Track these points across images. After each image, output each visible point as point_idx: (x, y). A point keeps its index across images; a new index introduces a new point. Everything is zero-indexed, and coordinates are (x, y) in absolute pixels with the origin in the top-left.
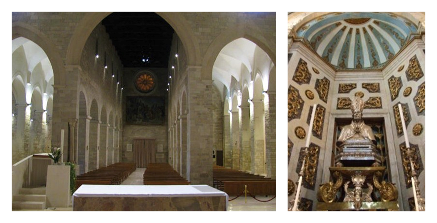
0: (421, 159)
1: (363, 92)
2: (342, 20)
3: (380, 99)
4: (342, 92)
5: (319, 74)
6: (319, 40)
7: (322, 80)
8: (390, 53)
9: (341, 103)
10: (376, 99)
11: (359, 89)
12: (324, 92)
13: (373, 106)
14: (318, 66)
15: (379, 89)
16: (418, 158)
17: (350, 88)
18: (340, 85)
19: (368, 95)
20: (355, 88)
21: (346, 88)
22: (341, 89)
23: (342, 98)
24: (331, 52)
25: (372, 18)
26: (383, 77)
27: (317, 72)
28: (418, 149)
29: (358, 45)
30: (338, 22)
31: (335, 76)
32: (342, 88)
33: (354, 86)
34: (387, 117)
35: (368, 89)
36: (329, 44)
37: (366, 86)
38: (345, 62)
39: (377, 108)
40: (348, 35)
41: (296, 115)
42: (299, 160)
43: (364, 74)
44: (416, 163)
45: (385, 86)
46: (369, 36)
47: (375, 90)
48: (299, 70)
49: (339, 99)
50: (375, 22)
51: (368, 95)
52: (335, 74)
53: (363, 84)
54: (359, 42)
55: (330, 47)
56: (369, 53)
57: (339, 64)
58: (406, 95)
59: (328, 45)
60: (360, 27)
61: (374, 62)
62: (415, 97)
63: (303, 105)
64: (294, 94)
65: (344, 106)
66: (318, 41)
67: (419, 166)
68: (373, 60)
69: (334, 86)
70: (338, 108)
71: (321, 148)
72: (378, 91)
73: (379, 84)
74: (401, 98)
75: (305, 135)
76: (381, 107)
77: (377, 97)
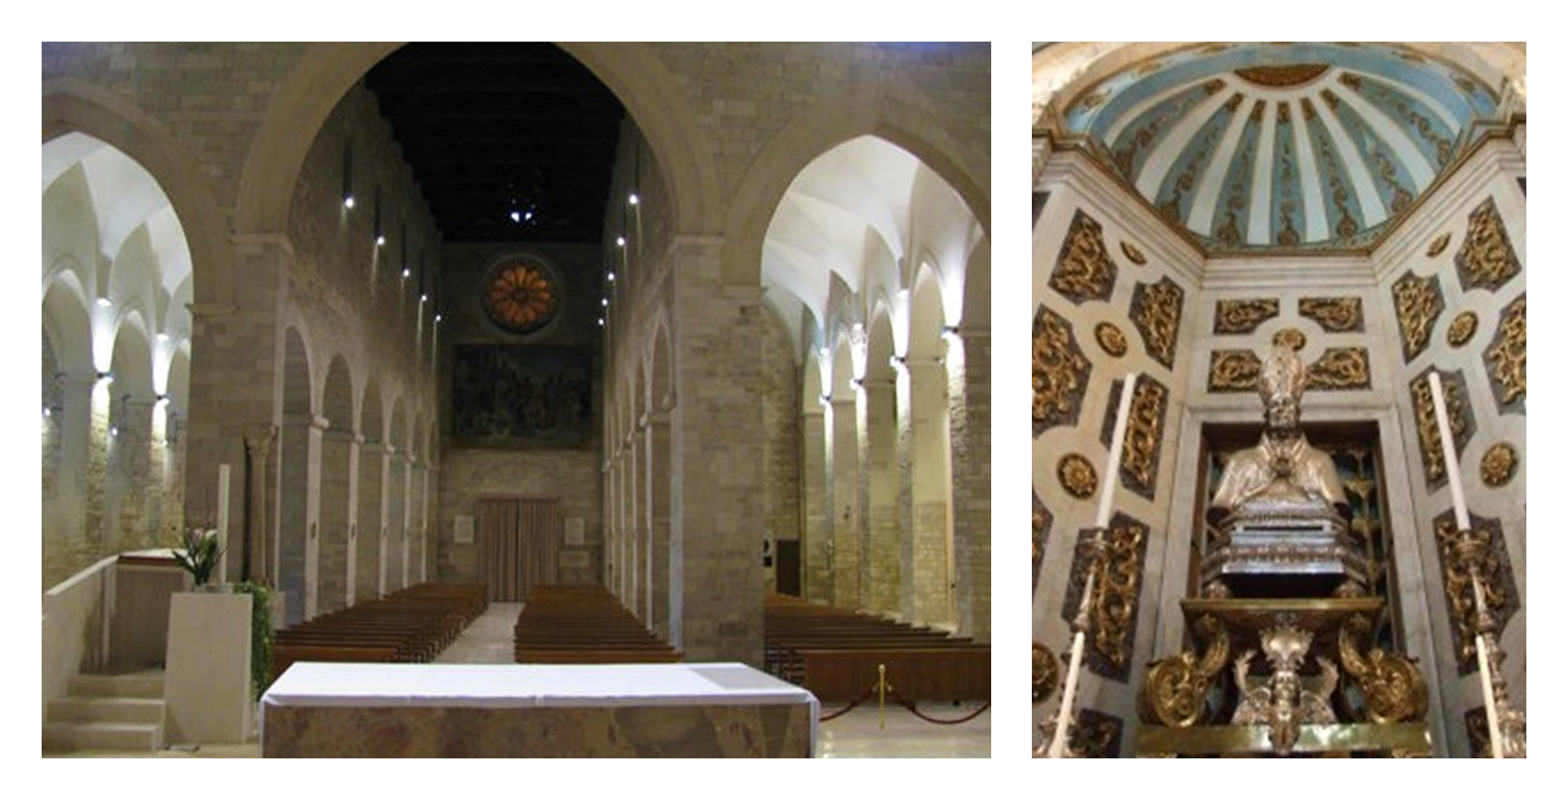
0: (1509, 570)
1: (1302, 329)
2: (1227, 70)
3: (1364, 353)
4: (1226, 332)
5: (1146, 267)
6: (1144, 144)
7: (1156, 287)
8: (1400, 191)
9: (1223, 368)
10: (1349, 357)
11: (1289, 318)
12: (1163, 330)
13: (1338, 382)
14: (1142, 237)
15: (1360, 319)
16: (1499, 567)
17: (1254, 315)
18: (1219, 305)
19: (1319, 342)
20: (1274, 314)
21: (1243, 317)
22: (1224, 319)
23: (1225, 352)
24: (1187, 188)
25: (1336, 64)
26: (1374, 276)
27: (1138, 260)
28: (1501, 535)
29: (1285, 161)
30: (1212, 78)
31: (1204, 271)
32: (1228, 314)
33: (1271, 309)
34: (1390, 418)
35: (1320, 320)
36: (1182, 157)
37: (1311, 309)
38: (1238, 223)
39: (1351, 386)
40: (1247, 124)
41: (1061, 412)
42: (1072, 576)
43: (1305, 265)
44: (1491, 586)
45: (1380, 310)
46: (1325, 129)
47: (1345, 322)
48: (1075, 250)
49: (1215, 355)
50: (1347, 80)
51: (1319, 342)
52: (1201, 265)
53: (1302, 302)
54: (1287, 151)
55: (1184, 170)
56: (1324, 189)
57: (1216, 228)
58: (1459, 339)
59: (1177, 163)
60: (1293, 96)
61: (1343, 222)
62: (1491, 347)
63: (1087, 377)
64: (1054, 336)
65: (1234, 380)
66: (1139, 147)
67: (1505, 596)
68: (1340, 217)
69: (1199, 309)
70: (1213, 389)
71: (1151, 531)
72: (1357, 326)
73: (1359, 301)
74: (1438, 352)
75: (1094, 486)
76: (1366, 385)
77: (1354, 349)
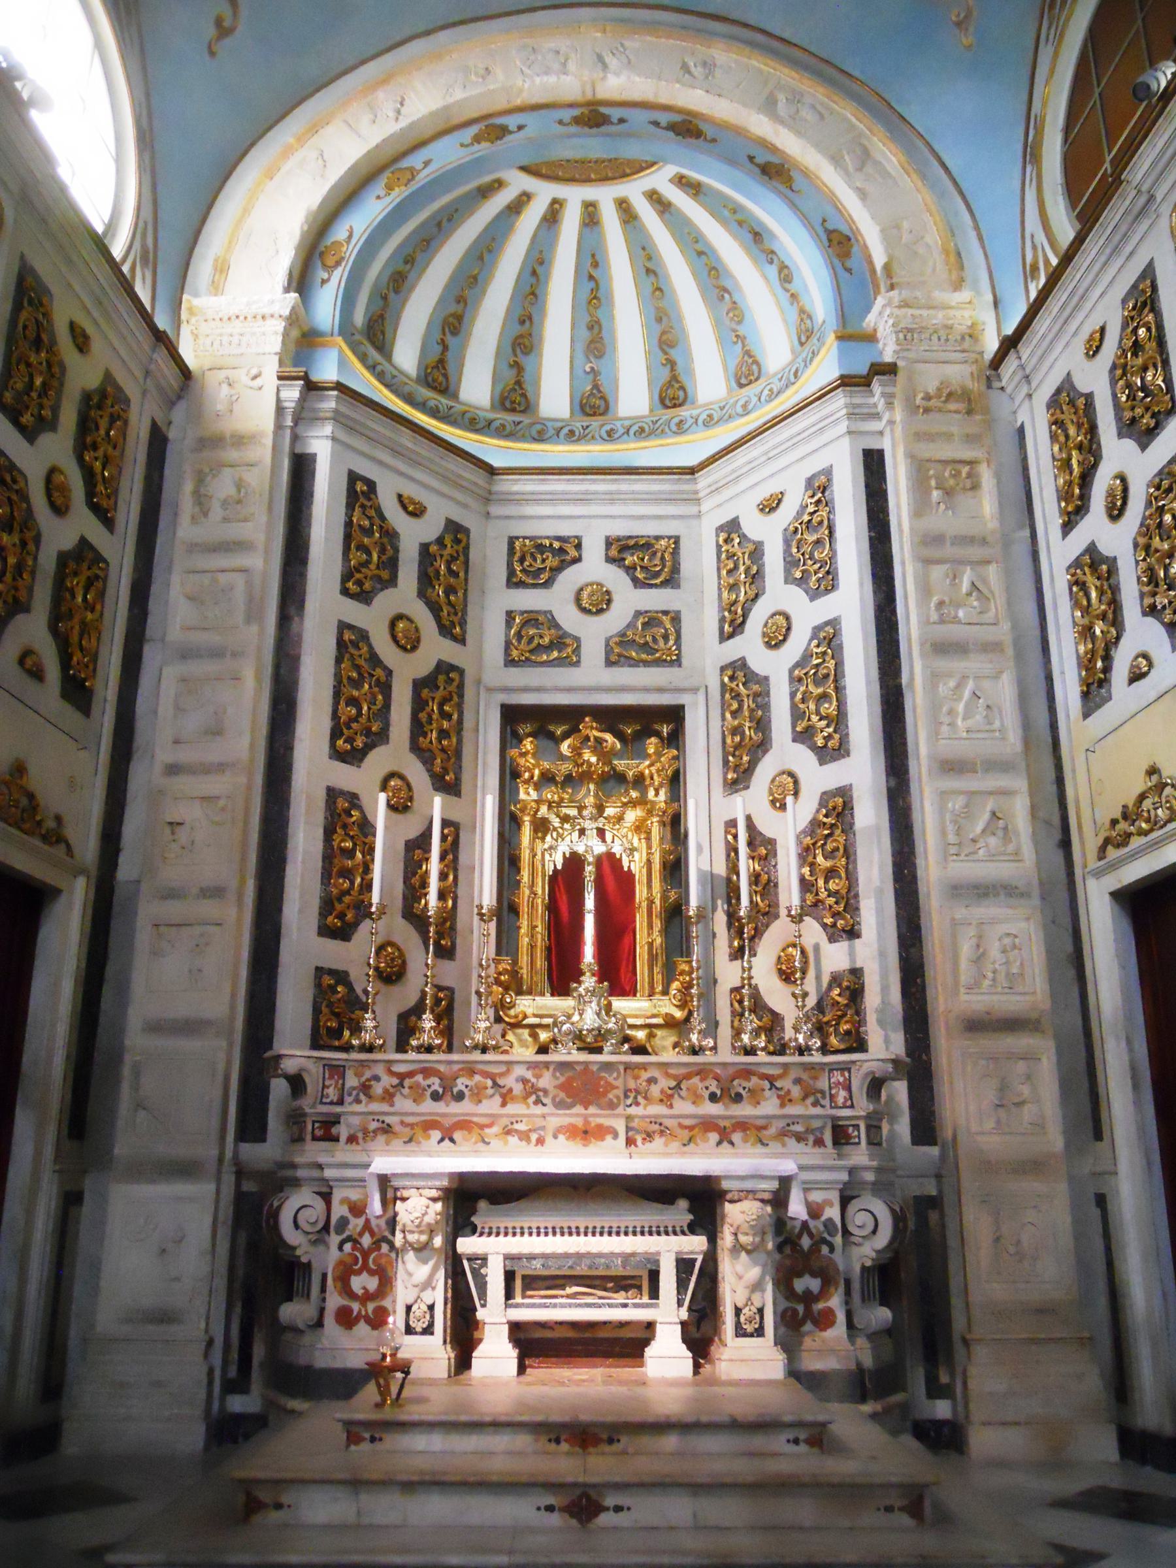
0: (776, 885)
1: (609, 585)
2: (510, 167)
3: (676, 619)
4: (521, 584)
5: (426, 516)
6: (397, 291)
7: (440, 541)
8: (748, 353)
9: (519, 636)
10: (660, 623)
11: (592, 567)
12: (452, 598)
13: (644, 656)
14: (419, 475)
15: (676, 569)
16: (769, 881)
17: (552, 561)
18: (512, 541)
19: (629, 600)
20: (577, 560)
21: (539, 565)
22: (518, 568)
23: (522, 613)
24: (455, 332)
25: (666, 162)
26: (698, 501)
27: (415, 511)
28: (775, 855)
29: (591, 277)
30: (487, 179)
31: (490, 493)
32: (522, 560)
33: (573, 553)
34: (695, 704)
35: (630, 570)
36: (447, 288)
37: (621, 550)
38: (527, 377)
39: (659, 662)
40: (539, 227)
41: (375, 734)
42: (405, 882)
43: (613, 487)
44: (761, 896)
45: (701, 562)
46: (648, 237)
47: (657, 575)
48: (357, 533)
49: (510, 616)
50: (681, 181)
51: (629, 600)
52: (486, 486)
53: (609, 542)
54: (596, 265)
55: (453, 308)
56: (646, 325)
57: (499, 389)
58: (775, 640)
59: (442, 301)
60: (605, 195)
61: (669, 385)
62: (797, 665)
63: (390, 687)
64: (355, 652)
65: (531, 651)
66: (392, 295)
67: (769, 906)
68: (664, 374)
69: (489, 557)
70: (510, 662)
71: (461, 827)
72: (672, 581)
73: (677, 540)
74: (749, 646)
75: (411, 799)
76: (678, 662)
77: (666, 613)
